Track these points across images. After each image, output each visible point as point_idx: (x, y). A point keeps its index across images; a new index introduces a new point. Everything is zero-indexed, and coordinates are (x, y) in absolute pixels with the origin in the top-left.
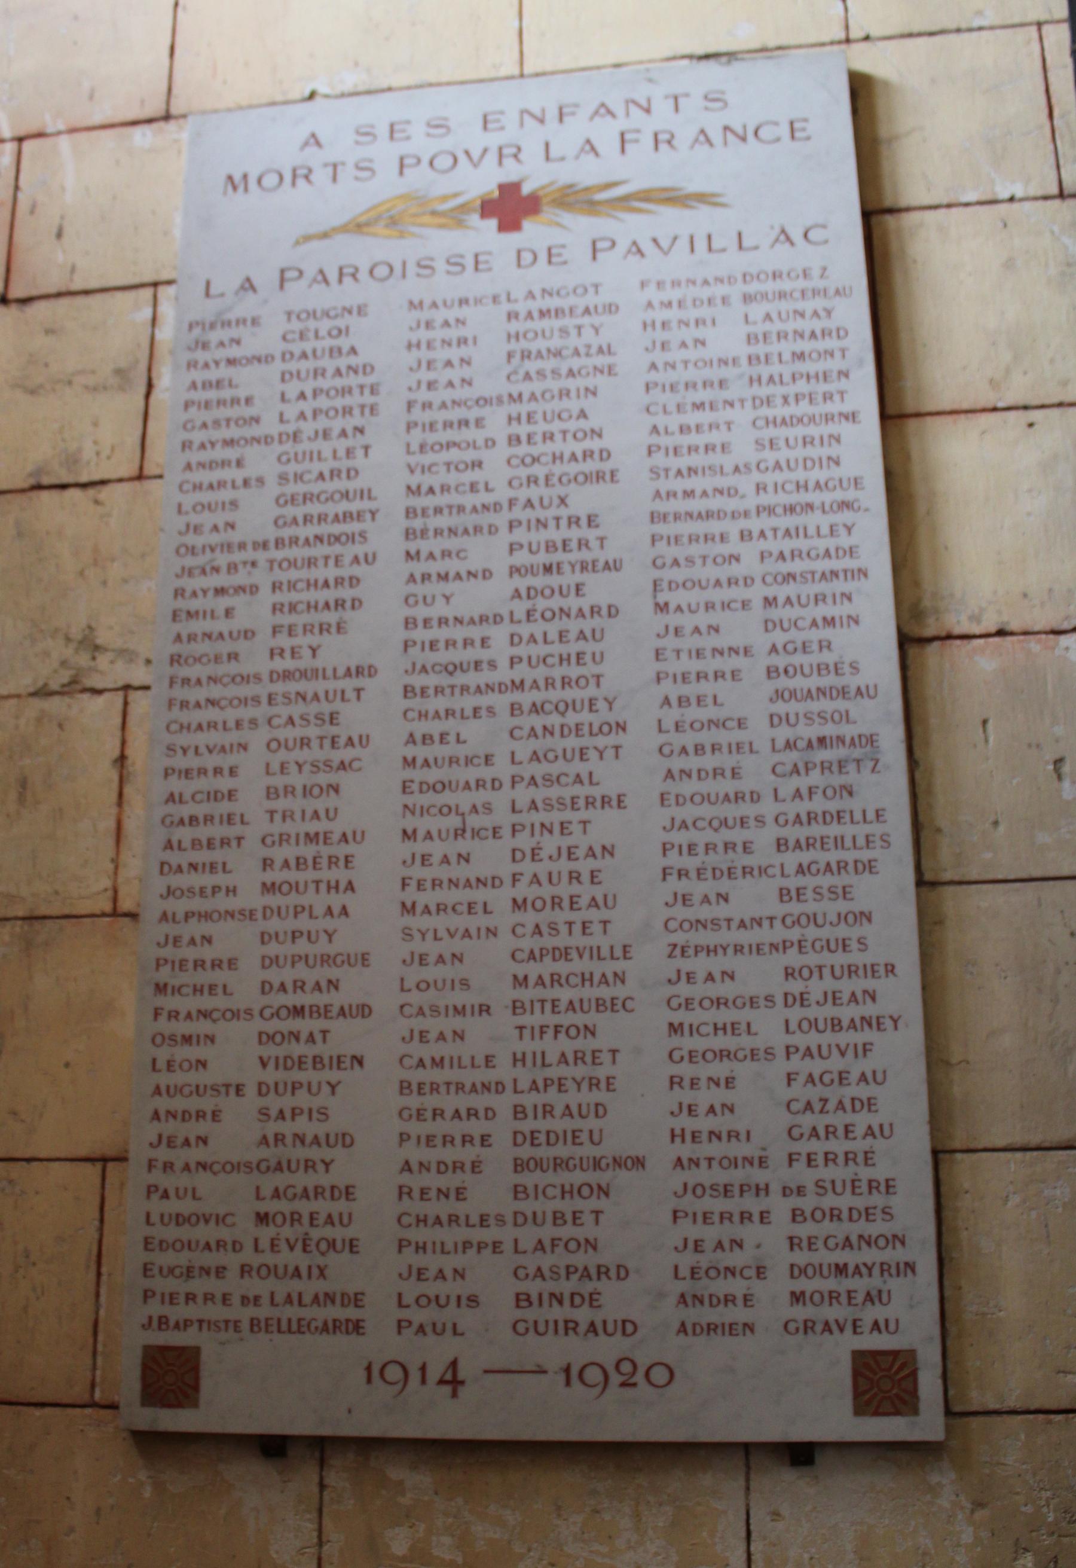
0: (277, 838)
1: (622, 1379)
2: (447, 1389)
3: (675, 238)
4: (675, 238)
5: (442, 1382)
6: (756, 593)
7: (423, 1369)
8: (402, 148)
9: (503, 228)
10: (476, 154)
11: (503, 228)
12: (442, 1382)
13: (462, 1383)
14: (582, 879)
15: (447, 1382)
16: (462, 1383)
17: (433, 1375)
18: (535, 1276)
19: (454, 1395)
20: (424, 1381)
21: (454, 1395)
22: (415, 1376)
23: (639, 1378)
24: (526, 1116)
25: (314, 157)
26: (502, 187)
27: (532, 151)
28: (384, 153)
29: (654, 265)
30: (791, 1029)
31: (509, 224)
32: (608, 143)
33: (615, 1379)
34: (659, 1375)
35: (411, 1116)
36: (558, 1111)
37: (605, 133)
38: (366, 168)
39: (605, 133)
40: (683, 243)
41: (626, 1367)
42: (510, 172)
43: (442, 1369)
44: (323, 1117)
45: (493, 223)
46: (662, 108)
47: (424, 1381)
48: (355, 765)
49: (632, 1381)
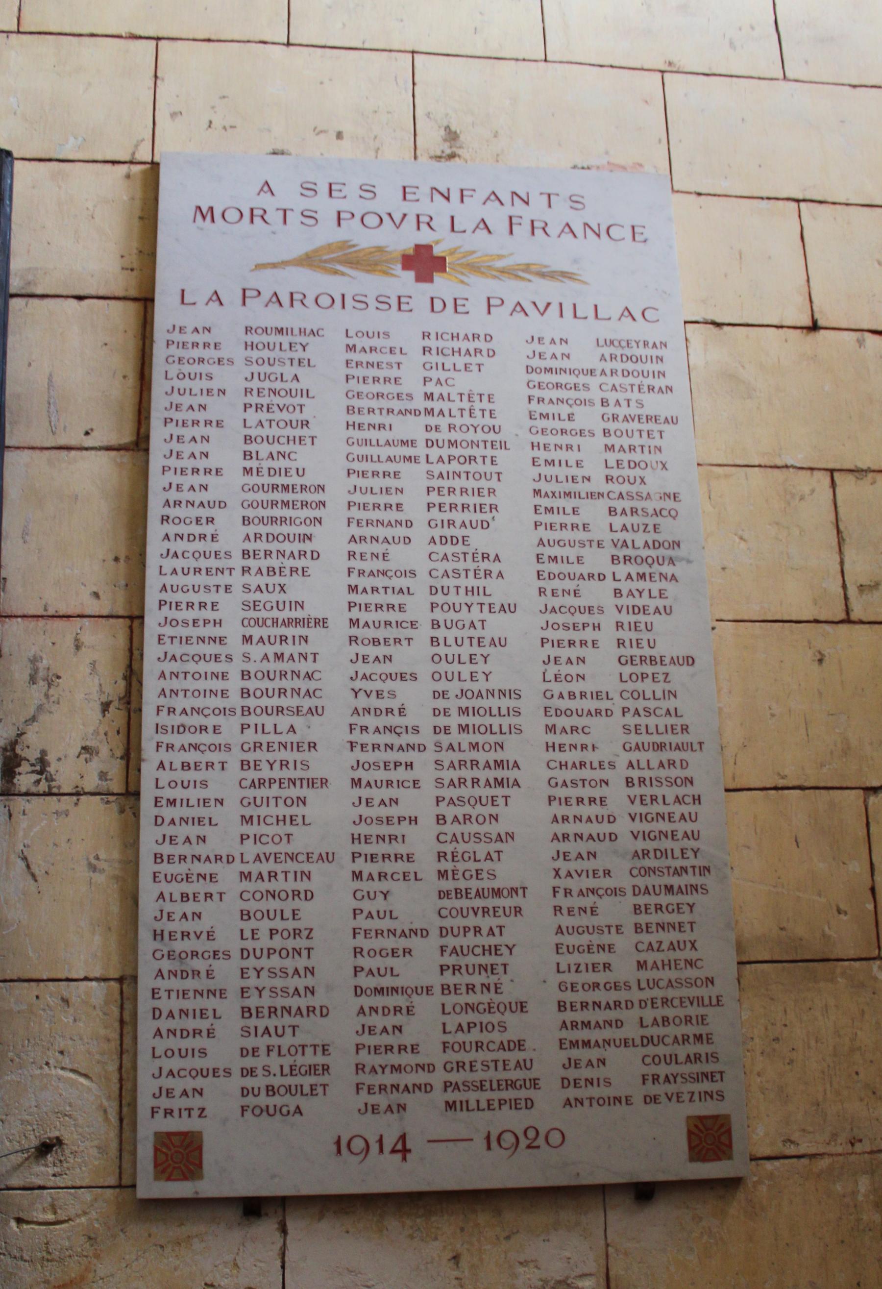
0: (252, 746)
1: (528, 1142)
2: (399, 1156)
3: (549, 304)
4: (549, 304)
5: (393, 1151)
6: (437, 1078)
7: (380, 1141)
8: (338, 204)
9: (419, 279)
10: (397, 218)
11: (419, 279)
12: (393, 1151)
13: (410, 1151)
14: (475, 989)
15: (398, 1151)
16: (410, 1151)
17: (387, 1147)
18: (496, 841)
19: (404, 1159)
20: (381, 1150)
21: (404, 1159)
22: (374, 1148)
23: (541, 1141)
24: (188, 899)
25: (265, 201)
26: (418, 247)
27: (442, 223)
28: (325, 207)
29: (534, 324)
30: (282, 1053)
31: (425, 277)
32: (499, 224)
33: (523, 1142)
34: (555, 1138)
35: (388, 954)
36: (458, 524)
37: (497, 217)
38: (310, 216)
39: (497, 217)
40: (555, 308)
41: (531, 1134)
42: (425, 237)
43: (394, 1141)
44: (227, 957)
45: (411, 275)
46: (538, 202)
47: (381, 1150)
48: (318, 693)
49: (535, 1144)
